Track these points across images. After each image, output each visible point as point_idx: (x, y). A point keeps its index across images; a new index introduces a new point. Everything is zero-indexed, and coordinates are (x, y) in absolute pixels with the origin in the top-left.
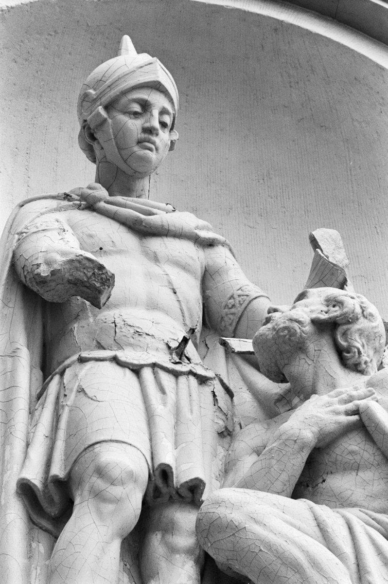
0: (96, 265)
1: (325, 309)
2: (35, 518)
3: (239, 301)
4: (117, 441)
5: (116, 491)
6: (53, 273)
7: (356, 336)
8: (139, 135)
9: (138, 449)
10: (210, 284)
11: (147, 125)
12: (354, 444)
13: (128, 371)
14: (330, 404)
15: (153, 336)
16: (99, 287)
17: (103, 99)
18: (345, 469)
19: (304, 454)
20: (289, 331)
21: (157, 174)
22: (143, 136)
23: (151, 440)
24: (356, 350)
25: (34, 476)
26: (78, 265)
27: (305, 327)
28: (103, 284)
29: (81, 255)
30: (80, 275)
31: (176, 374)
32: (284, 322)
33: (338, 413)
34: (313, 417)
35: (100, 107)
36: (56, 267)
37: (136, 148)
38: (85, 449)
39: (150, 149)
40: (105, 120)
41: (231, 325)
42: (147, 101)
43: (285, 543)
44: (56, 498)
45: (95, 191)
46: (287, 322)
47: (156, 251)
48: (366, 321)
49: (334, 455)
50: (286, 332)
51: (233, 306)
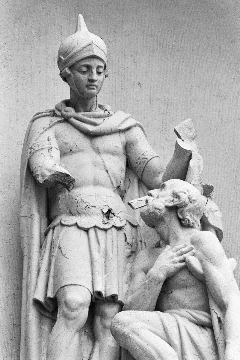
0: (65, 175)
1: (172, 199)
2: (43, 312)
3: (143, 161)
4: (74, 285)
5: (74, 314)
6: (45, 181)
7: (187, 213)
8: (87, 83)
9: (85, 287)
10: (129, 149)
11: (90, 78)
12: (184, 277)
13: (82, 232)
14: (172, 257)
15: (95, 206)
16: (68, 185)
17: (68, 64)
18: (181, 288)
19: (160, 285)
20: (155, 214)
21: (115, 32)
22: (89, 83)
23: (92, 275)
24: (187, 220)
25: (40, 297)
26: (56, 176)
27: (162, 211)
28: (69, 183)
29: (58, 171)
30: (58, 179)
31: (106, 230)
32: (152, 209)
33: (175, 262)
34: (164, 266)
35: (67, 68)
36: (46, 178)
37: (86, 89)
38: (61, 288)
39: (94, 89)
40: (70, 75)
41: (140, 172)
42: (89, 65)
43: (147, 346)
44: (51, 305)
45: (67, 113)
46: (154, 209)
47: (98, 147)
48: (191, 204)
49: (175, 281)
50: (153, 214)
51: (140, 163)
